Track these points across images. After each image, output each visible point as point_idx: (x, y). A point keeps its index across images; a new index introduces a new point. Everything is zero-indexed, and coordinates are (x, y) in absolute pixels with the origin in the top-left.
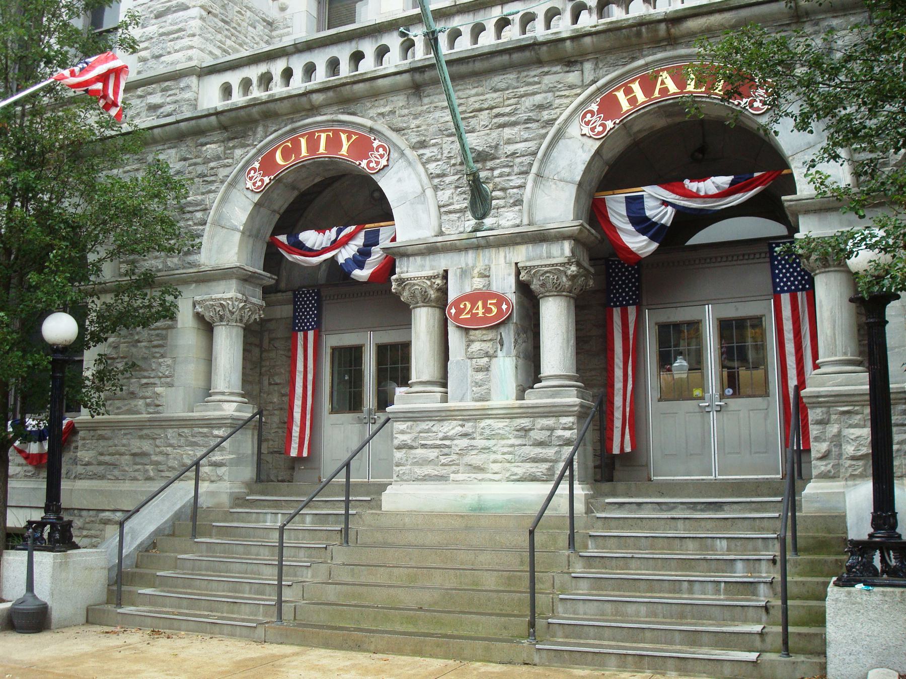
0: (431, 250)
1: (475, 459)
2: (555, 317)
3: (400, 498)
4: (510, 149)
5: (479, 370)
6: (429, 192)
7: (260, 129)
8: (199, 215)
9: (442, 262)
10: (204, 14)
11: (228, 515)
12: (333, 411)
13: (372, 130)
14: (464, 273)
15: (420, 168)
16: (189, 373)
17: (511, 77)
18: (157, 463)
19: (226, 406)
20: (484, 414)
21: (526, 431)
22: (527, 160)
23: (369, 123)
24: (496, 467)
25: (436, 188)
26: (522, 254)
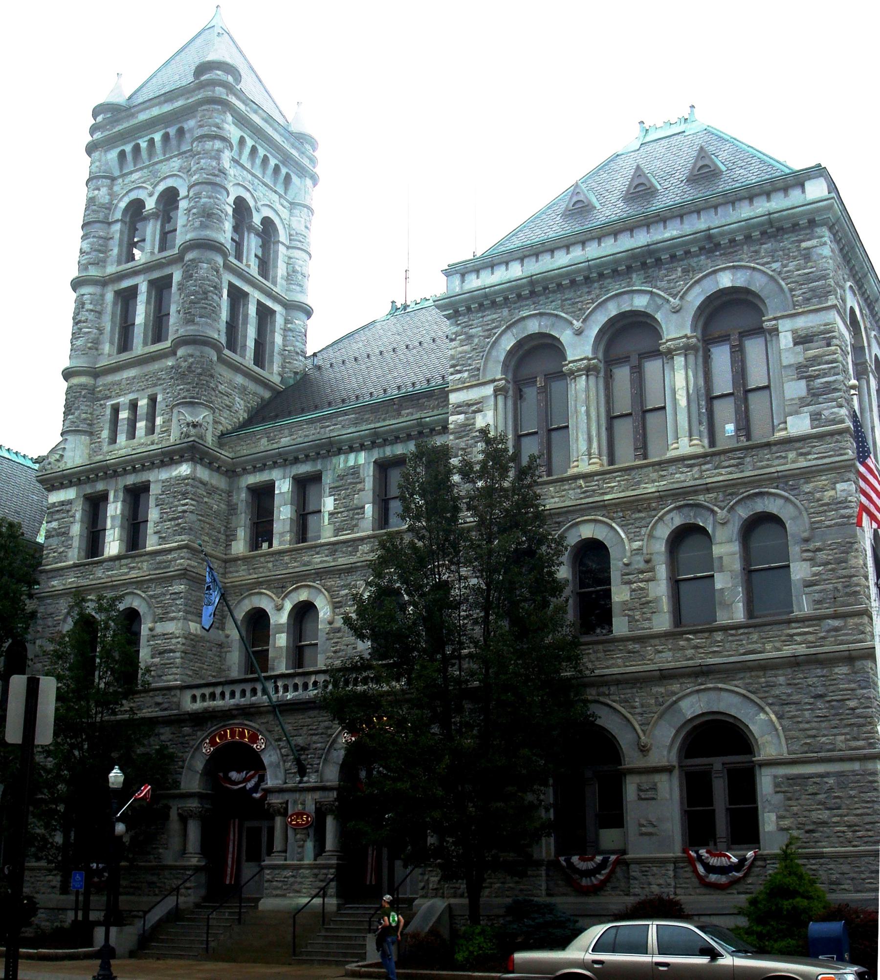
0: (281, 791)
1: (296, 887)
2: (330, 823)
3: (267, 904)
4: (315, 746)
5: (299, 847)
6: (281, 763)
7: (209, 723)
8: (180, 763)
9: (286, 796)
10: (183, 655)
11: (192, 912)
12: (247, 861)
13: (258, 730)
14: (295, 802)
15: (278, 751)
16: (175, 843)
17: (316, 712)
18: (160, 887)
19: (193, 860)
20: (300, 867)
21: (316, 875)
22: (320, 752)
23: (257, 726)
24: (304, 890)
25: (284, 762)
26: (317, 795)
